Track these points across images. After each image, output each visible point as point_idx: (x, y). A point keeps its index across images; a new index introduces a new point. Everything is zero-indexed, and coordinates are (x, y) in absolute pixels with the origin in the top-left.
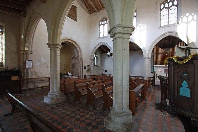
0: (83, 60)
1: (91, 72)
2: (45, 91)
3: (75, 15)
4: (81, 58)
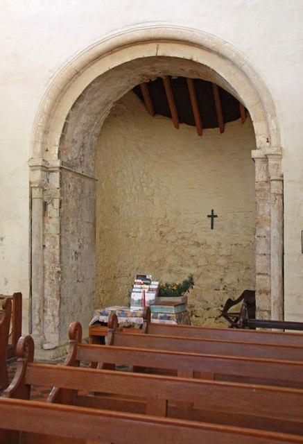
4: (265, 159)
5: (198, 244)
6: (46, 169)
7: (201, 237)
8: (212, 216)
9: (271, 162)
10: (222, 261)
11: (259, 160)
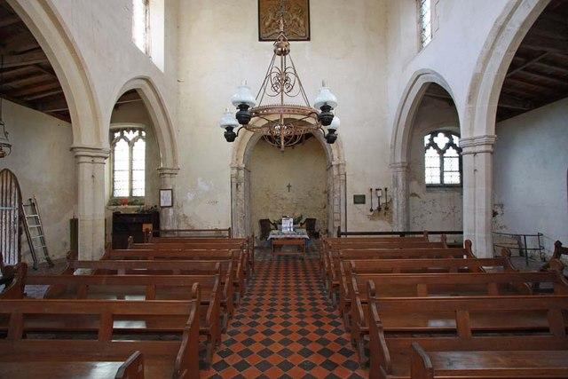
0: (349, 170)
1: (394, 217)
2: (202, 181)
3: (302, 23)
4: (338, 165)
5: (283, 199)
6: (239, 169)
7: (285, 195)
8: (289, 186)
9: (341, 166)
10: (294, 206)
11: (483, 154)
